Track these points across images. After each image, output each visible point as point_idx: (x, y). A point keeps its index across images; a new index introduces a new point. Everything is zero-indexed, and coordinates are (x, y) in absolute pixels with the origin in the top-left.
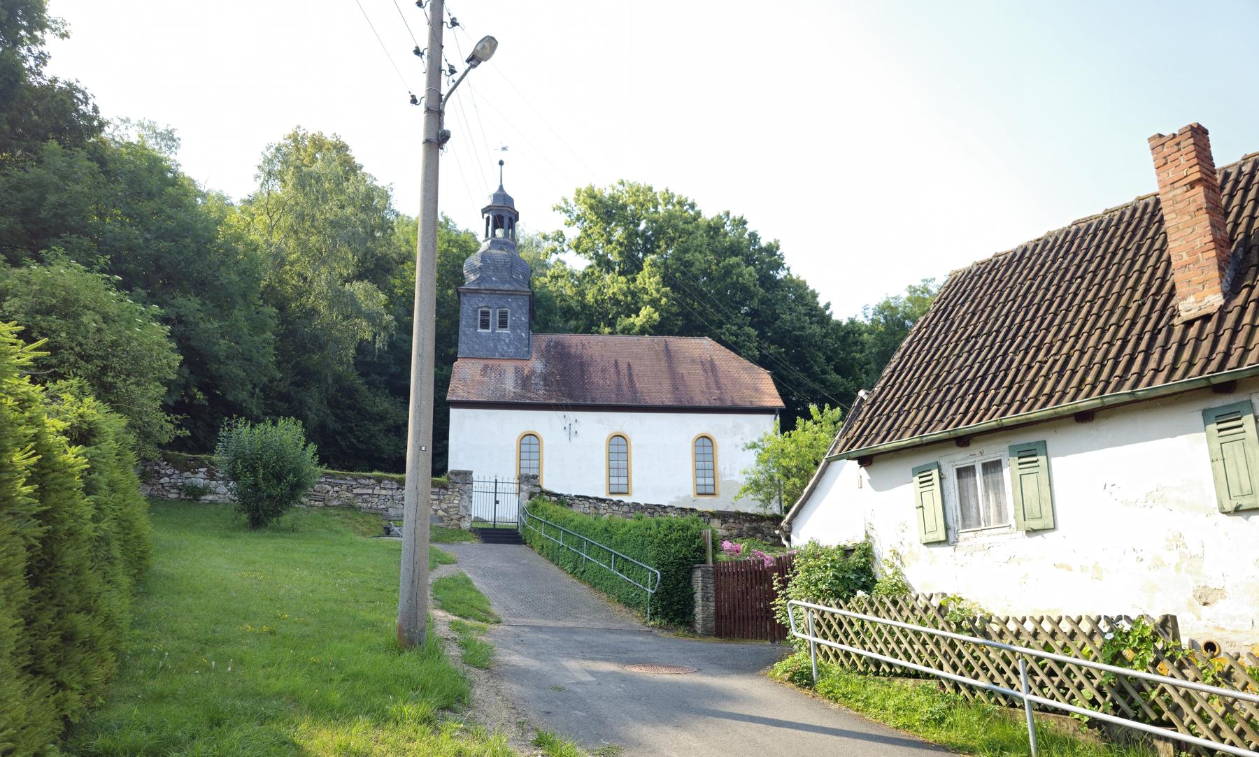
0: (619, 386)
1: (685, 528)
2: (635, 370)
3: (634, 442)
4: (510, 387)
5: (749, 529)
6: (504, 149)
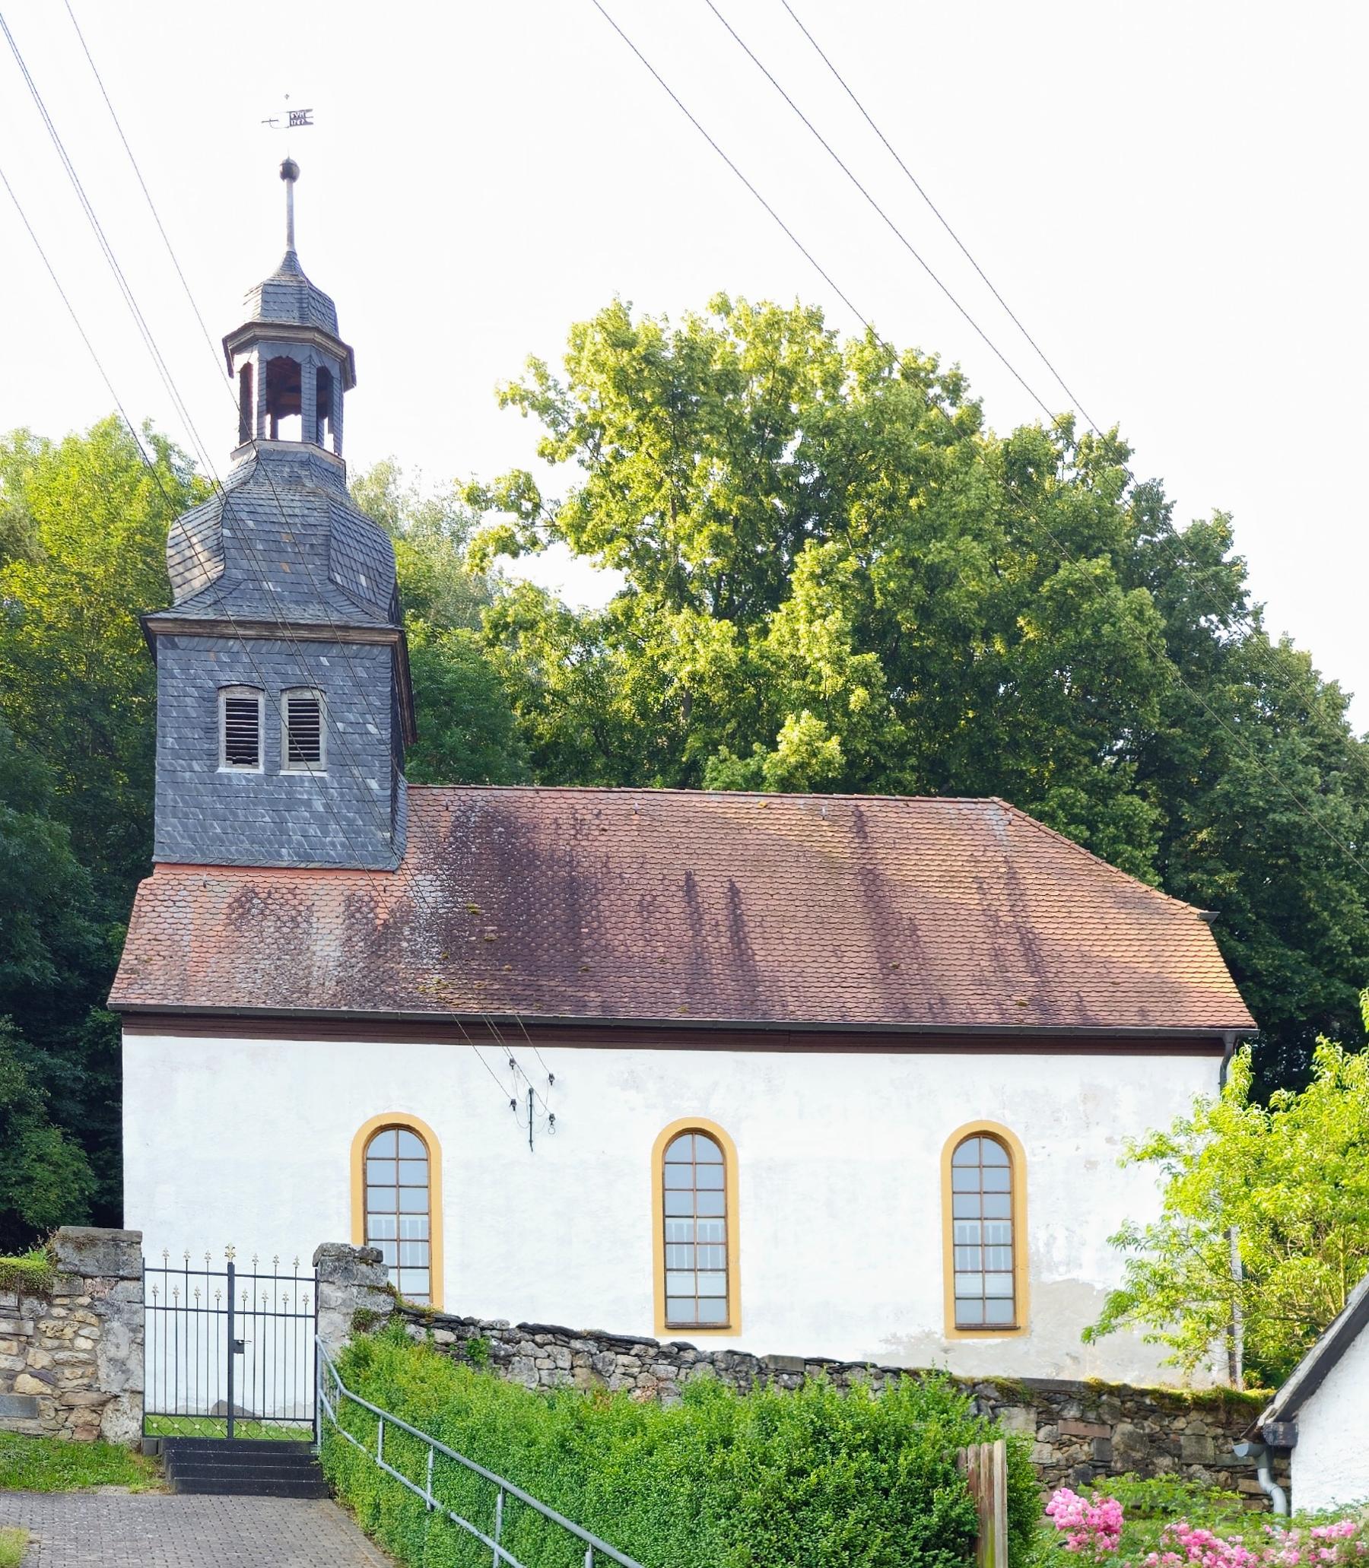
0: (698, 964)
1: (885, 1440)
2: (754, 906)
3: (748, 1151)
4: (327, 952)
5: (1131, 1442)
6: (299, 119)
